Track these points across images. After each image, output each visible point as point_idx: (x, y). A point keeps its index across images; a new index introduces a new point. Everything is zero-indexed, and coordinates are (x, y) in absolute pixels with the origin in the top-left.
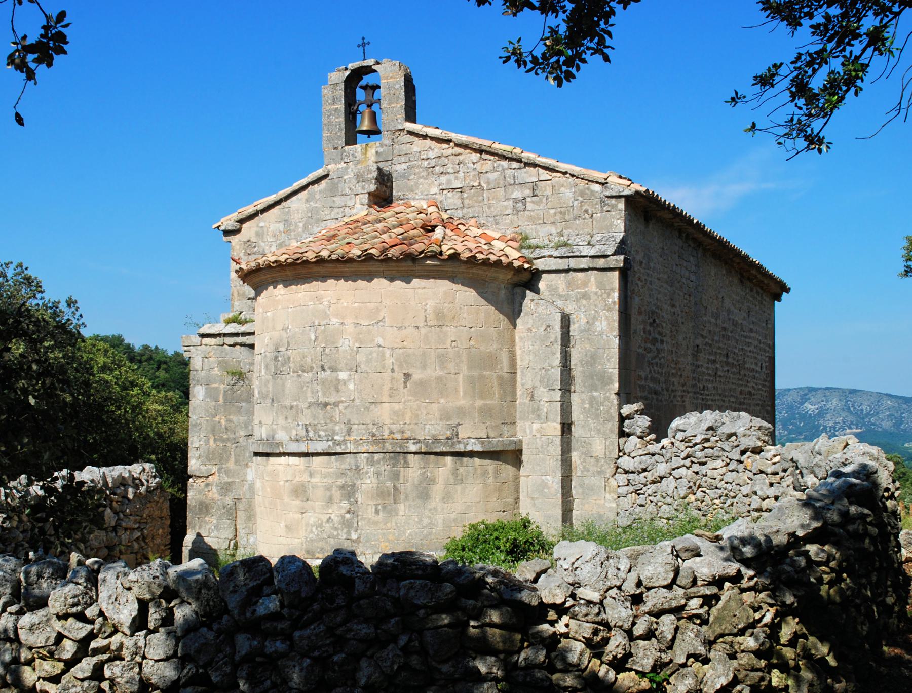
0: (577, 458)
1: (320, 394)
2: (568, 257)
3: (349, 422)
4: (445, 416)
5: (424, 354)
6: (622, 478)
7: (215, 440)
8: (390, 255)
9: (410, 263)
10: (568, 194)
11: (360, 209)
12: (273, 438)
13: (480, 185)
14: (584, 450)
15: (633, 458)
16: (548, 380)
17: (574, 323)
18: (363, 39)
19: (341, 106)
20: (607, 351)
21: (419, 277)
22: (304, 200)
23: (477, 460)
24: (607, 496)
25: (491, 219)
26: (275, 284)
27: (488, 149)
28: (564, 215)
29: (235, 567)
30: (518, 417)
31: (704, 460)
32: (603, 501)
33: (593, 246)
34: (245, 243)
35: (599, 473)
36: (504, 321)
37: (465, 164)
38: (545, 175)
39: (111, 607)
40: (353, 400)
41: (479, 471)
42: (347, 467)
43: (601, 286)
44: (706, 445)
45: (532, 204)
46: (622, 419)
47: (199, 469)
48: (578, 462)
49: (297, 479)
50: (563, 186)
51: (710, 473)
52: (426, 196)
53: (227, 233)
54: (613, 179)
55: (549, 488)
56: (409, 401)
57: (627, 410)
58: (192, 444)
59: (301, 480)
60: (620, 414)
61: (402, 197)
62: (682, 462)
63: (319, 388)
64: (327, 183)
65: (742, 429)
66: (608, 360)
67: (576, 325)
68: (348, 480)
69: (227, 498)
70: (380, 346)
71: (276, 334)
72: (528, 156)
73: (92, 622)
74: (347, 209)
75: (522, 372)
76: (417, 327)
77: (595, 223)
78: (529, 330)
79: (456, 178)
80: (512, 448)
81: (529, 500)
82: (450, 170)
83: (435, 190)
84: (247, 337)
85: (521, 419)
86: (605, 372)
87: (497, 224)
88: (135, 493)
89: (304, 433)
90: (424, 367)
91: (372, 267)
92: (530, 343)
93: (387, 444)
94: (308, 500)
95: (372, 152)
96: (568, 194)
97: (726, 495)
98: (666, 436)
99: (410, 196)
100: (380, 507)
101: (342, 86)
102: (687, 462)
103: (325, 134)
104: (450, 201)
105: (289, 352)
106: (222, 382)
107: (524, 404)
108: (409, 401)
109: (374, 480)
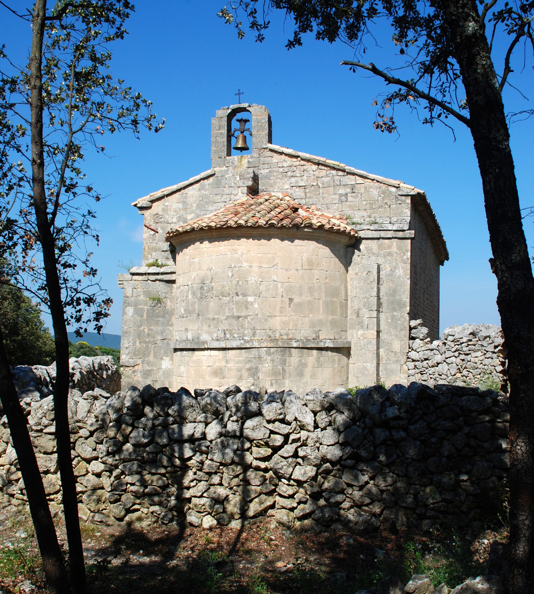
0: (383, 352)
1: (235, 310)
2: (380, 230)
3: (254, 328)
4: (312, 325)
5: (301, 286)
6: (411, 365)
7: (140, 342)
8: (285, 225)
9: (295, 230)
10: (375, 192)
11: (242, 197)
12: (198, 338)
13: (317, 184)
14: (387, 348)
15: (418, 352)
16: (369, 305)
17: (382, 270)
18: (239, 90)
19: (224, 131)
20: (403, 288)
21: (299, 239)
22: (197, 189)
23: (329, 353)
24: (402, 376)
25: (325, 206)
26: (201, 241)
27: (324, 163)
28: (372, 205)
29: (371, 390)
30: (348, 327)
31: (469, 352)
32: (399, 379)
33: (394, 224)
34: (154, 215)
35: (397, 361)
36: (335, 262)
37: (308, 171)
38: (360, 180)
39: (300, 415)
40: (257, 315)
41: (330, 360)
42: (253, 356)
43: (399, 248)
44: (469, 343)
45: (351, 198)
46: (411, 329)
47: (128, 361)
48: (384, 355)
49: (217, 364)
50: (371, 187)
51: (473, 360)
52: (281, 190)
53: (142, 208)
54: (402, 185)
55: (368, 371)
56: (292, 315)
57: (413, 323)
58: (123, 345)
59: (219, 365)
60: (410, 326)
61: (265, 190)
62: (453, 354)
63: (234, 306)
64: (214, 179)
65: (493, 333)
66: (403, 293)
67: (384, 272)
68: (253, 364)
69: (148, 380)
70: (275, 281)
71: (202, 273)
72: (348, 168)
73: (289, 424)
74: (232, 196)
75: (351, 299)
76: (297, 270)
77: (392, 211)
78: (357, 274)
79: (302, 180)
80: (347, 346)
81: (355, 378)
82: (298, 175)
83: (287, 186)
84: (165, 275)
85: (351, 328)
86: (401, 300)
87: (328, 209)
88: (107, 374)
89: (223, 335)
90: (301, 295)
91: (272, 231)
92: (357, 282)
93: (279, 342)
94: (224, 378)
95: (245, 161)
96: (374, 193)
97: (484, 373)
98: (438, 338)
99: (270, 190)
100: (273, 382)
101: (226, 119)
102: (456, 354)
103: (213, 148)
104: (297, 194)
105: (213, 284)
106: (146, 304)
107: (353, 319)
108: (292, 315)
109: (270, 365)
